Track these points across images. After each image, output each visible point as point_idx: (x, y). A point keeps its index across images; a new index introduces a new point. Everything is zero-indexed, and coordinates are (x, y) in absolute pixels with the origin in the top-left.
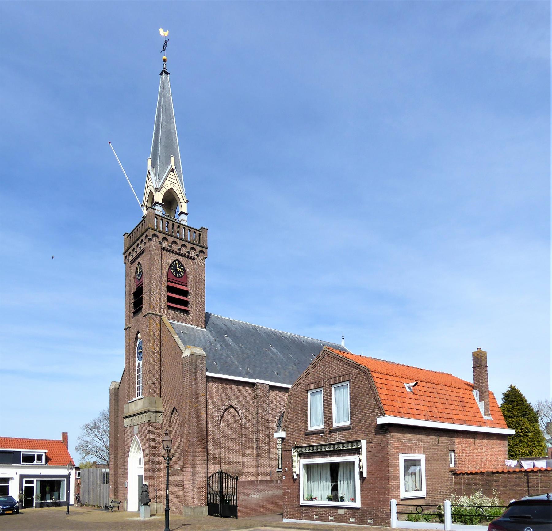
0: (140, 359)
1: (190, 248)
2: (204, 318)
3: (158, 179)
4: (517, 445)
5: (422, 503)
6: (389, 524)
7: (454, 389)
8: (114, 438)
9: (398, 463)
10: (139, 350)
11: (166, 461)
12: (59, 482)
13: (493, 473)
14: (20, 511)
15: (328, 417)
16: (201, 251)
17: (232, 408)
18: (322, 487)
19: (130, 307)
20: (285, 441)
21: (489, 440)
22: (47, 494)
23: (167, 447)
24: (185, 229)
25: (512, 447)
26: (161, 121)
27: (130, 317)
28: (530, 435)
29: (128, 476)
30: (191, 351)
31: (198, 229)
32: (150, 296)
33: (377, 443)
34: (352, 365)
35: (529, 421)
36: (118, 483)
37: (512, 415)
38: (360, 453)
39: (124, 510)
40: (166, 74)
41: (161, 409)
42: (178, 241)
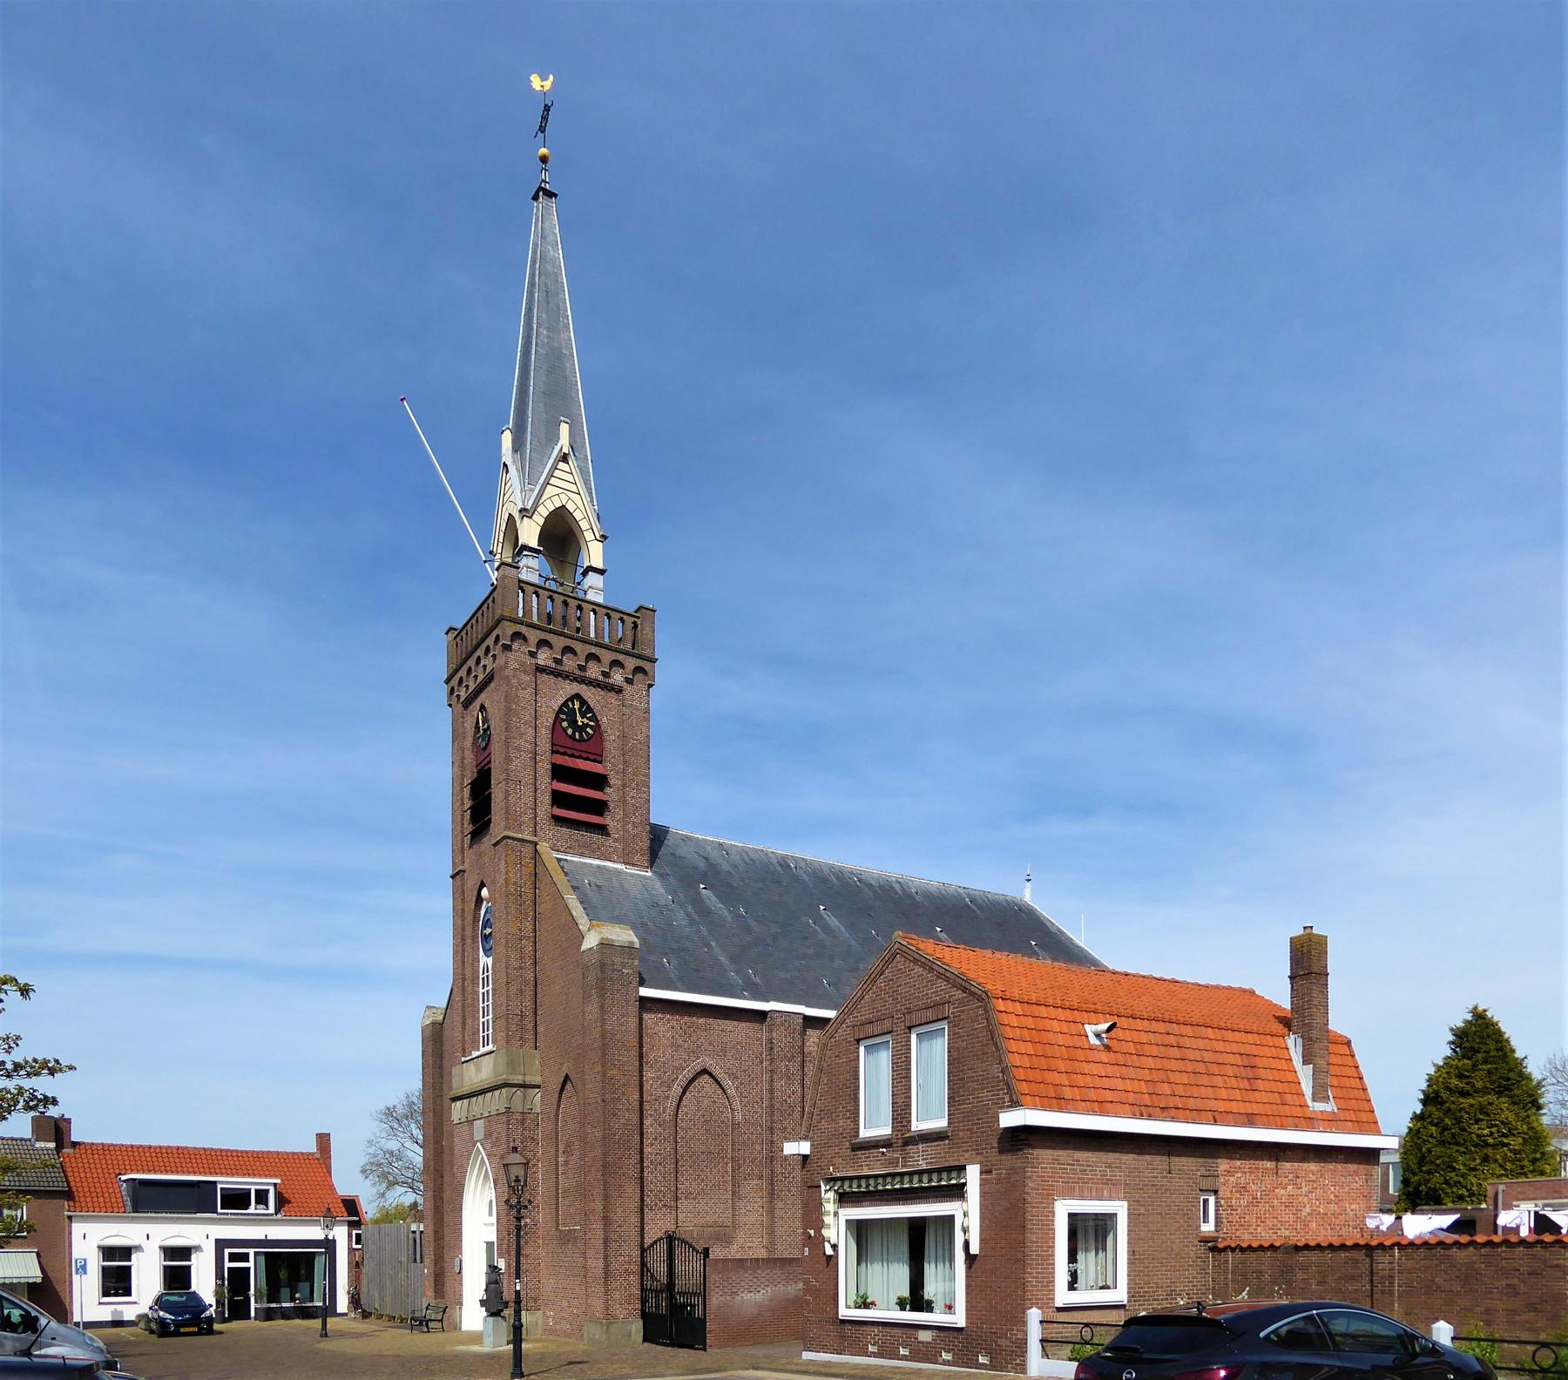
0: (487, 952)
2: (646, 844)
3: (526, 484)
4: (1474, 1169)
5: (1117, 1319)
6: (1022, 1368)
7: (1229, 1035)
9: (1053, 1221)
11: (514, 1212)
13: (1297, 1248)
14: (216, 1327)
15: (900, 1106)
16: (638, 670)
18: (891, 1276)
19: (462, 819)
21: (1322, 1165)
22: (300, 1281)
23: (517, 1180)
24: (595, 613)
25: (1463, 1176)
27: (463, 848)
28: (1512, 1143)
29: (463, 1243)
30: (602, 936)
31: (631, 611)
32: (507, 794)
33: (1002, 1173)
34: (954, 981)
35: (1514, 1103)
37: (1468, 1088)
38: (964, 1197)
40: (546, 197)
41: (537, 1080)
42: (578, 646)
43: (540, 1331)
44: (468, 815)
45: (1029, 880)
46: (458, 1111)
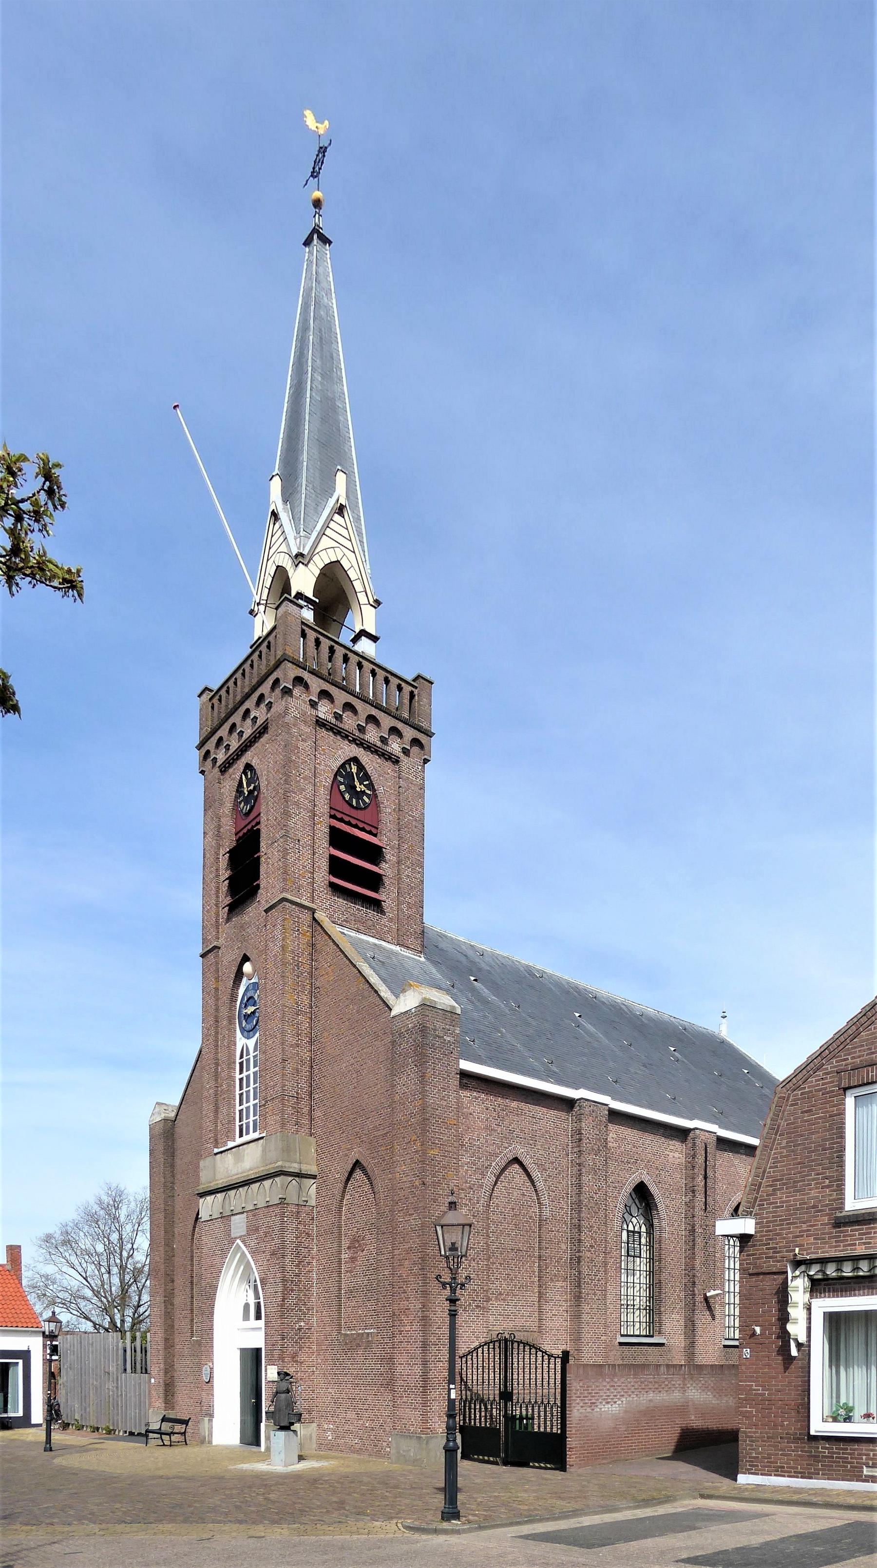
0: (248, 1033)
1: (389, 728)
8: (163, 1252)
10: (246, 1007)
11: (447, 1292)
12: (6, 1367)
16: (416, 742)
17: (518, 1167)
19: (218, 892)
20: (754, 1246)
26: (310, 369)
27: (217, 921)
30: (424, 996)
31: (409, 678)
32: (285, 853)
36: (175, 1371)
39: (202, 1442)
40: (320, 242)
41: (313, 1169)
43: (314, 1446)
44: (225, 885)
45: (724, 1017)
46: (208, 1207)
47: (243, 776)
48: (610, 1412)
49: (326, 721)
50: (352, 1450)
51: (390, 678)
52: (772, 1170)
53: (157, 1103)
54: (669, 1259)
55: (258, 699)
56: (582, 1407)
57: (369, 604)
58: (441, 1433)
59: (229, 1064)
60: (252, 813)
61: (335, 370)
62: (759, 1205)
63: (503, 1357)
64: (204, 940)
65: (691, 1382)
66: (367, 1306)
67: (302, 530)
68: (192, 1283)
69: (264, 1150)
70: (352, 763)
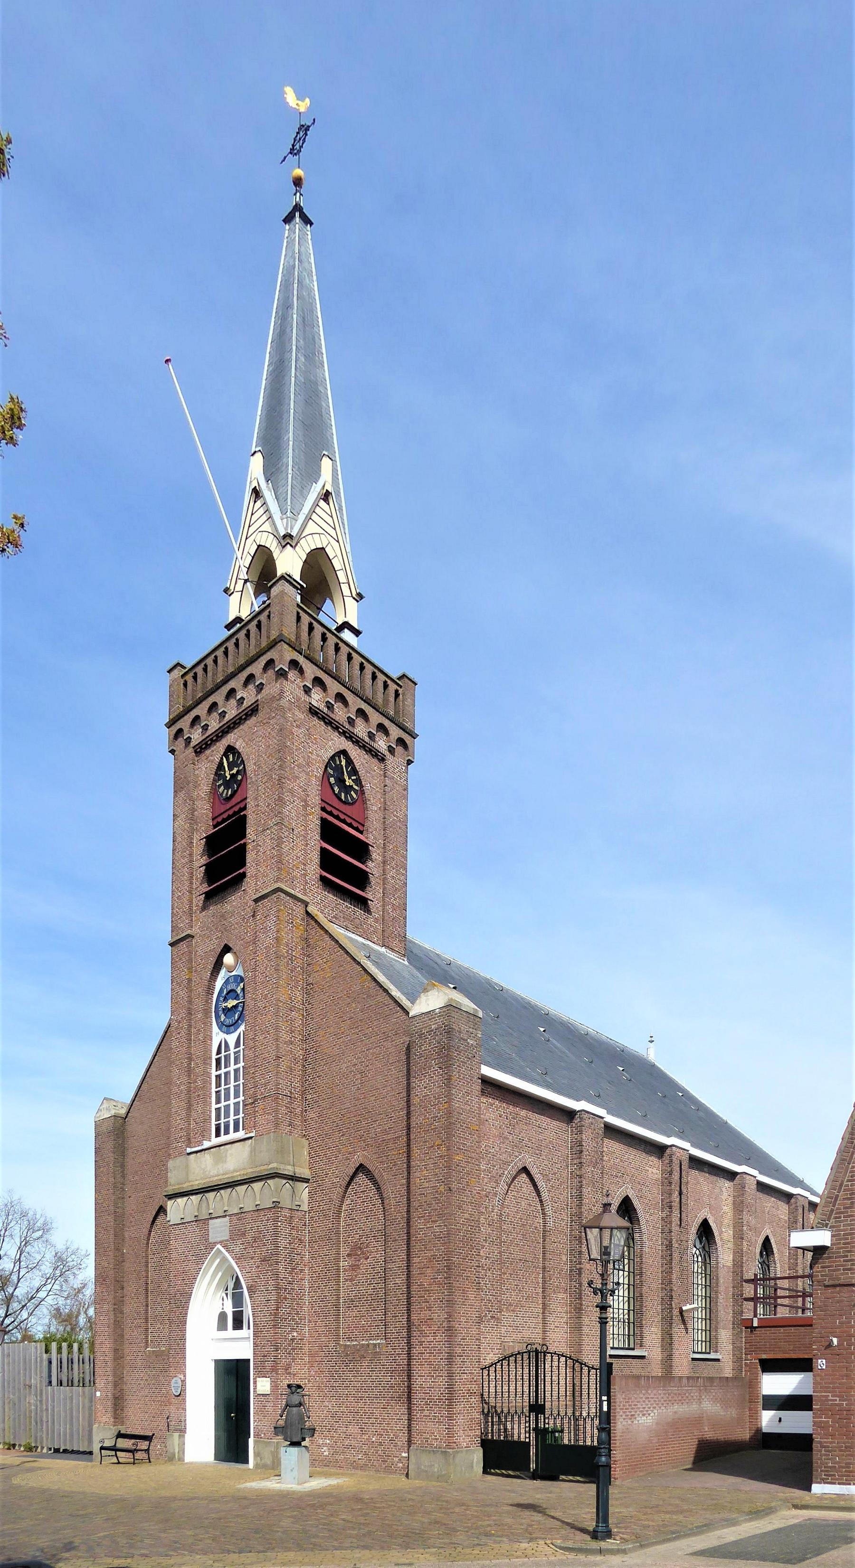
10: (226, 999)
16: (401, 742)
17: (525, 1176)
20: (830, 1258)
26: (294, 348)
27: (191, 908)
31: (395, 676)
32: (279, 842)
39: (171, 1459)
41: (305, 1172)
45: (651, 1042)
46: (177, 1210)
47: (224, 758)
48: (646, 1424)
49: (319, 709)
50: (355, 1466)
51: (377, 674)
52: (850, 1183)
53: (105, 1099)
54: (648, 1273)
55: (246, 680)
56: (624, 1419)
57: (352, 596)
58: (465, 1447)
59: (204, 1060)
60: (233, 799)
61: (317, 353)
62: (836, 1218)
63: (533, 1369)
64: (174, 929)
65: (705, 1394)
66: (373, 1316)
67: (289, 511)
68: (147, 1290)
69: (253, 1150)
70: (342, 756)
